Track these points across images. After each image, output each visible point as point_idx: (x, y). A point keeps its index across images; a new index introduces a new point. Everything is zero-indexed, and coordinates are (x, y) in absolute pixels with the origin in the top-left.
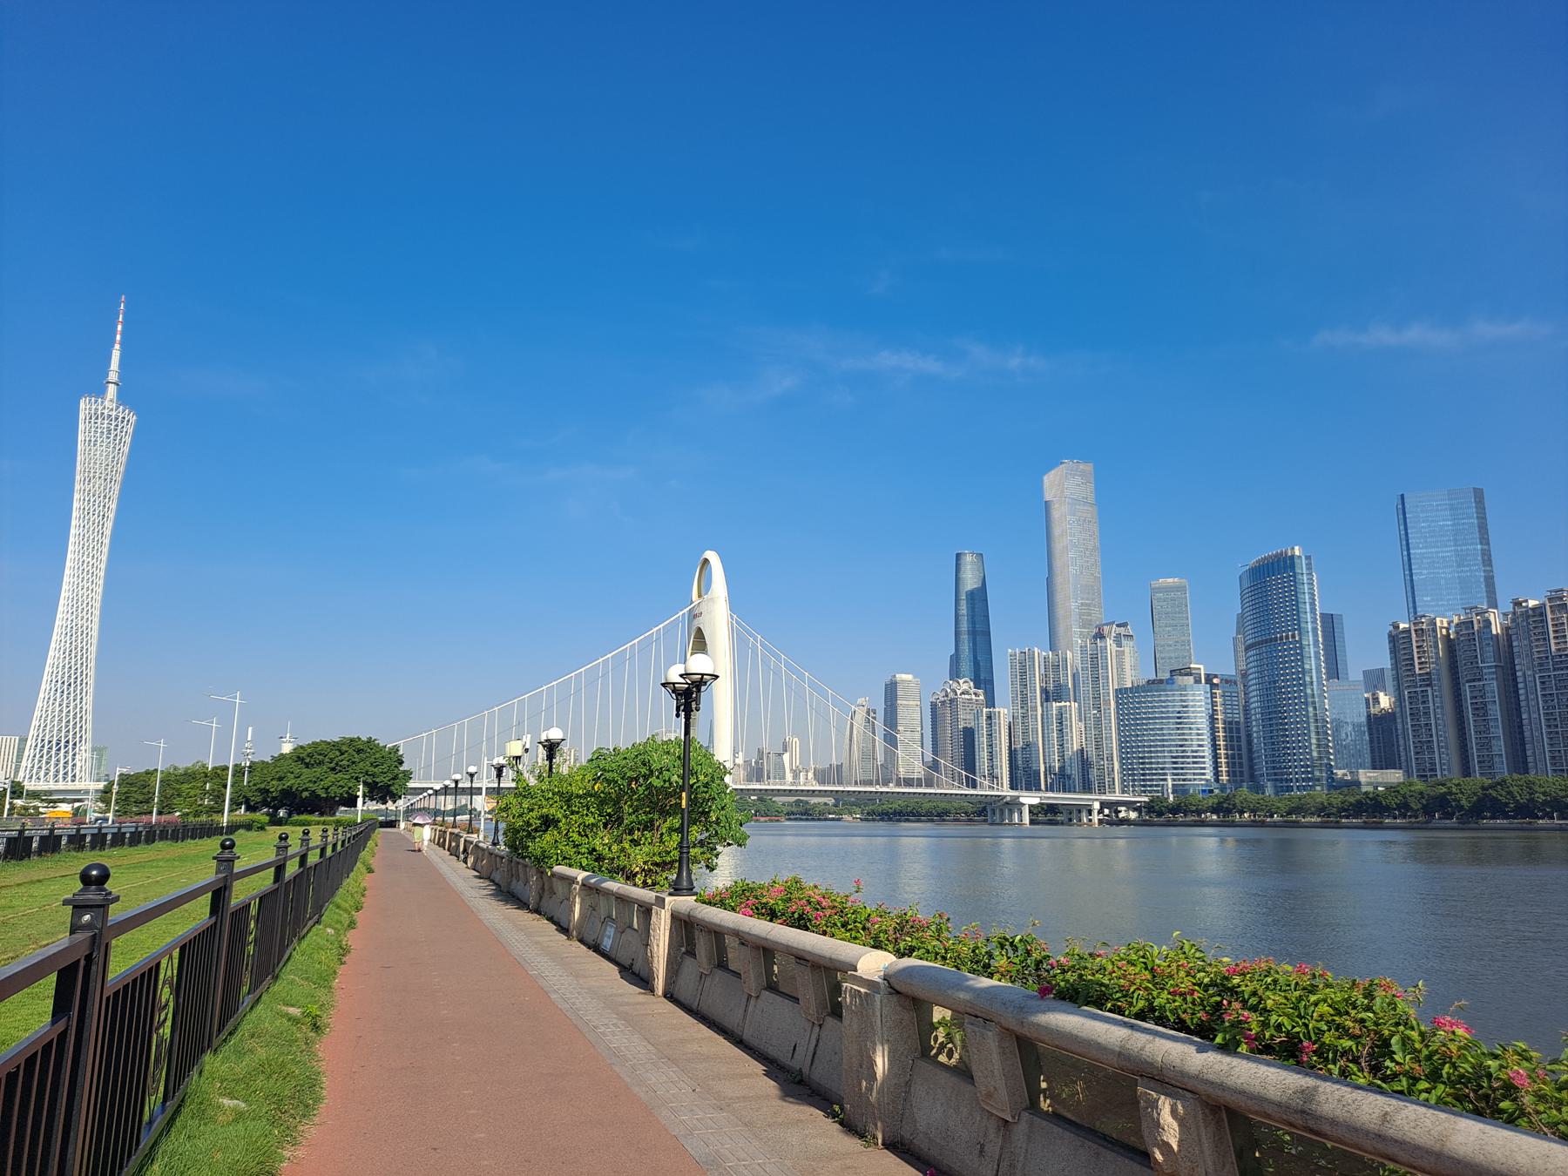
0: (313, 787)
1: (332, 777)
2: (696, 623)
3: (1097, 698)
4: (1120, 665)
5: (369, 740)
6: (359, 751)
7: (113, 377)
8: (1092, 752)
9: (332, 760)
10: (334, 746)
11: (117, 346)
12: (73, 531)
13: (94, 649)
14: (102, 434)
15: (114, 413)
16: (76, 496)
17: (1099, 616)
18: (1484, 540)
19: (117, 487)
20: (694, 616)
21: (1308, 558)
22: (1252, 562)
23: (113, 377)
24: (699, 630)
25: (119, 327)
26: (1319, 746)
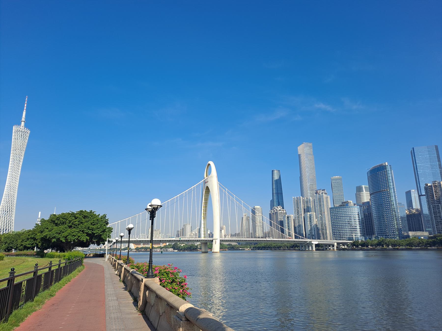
0: (58, 236)
1: (69, 230)
2: (206, 185)
3: (321, 211)
4: (327, 201)
5: (91, 212)
6: (85, 217)
7: (23, 119)
8: (319, 226)
9: (70, 221)
10: (73, 215)
11: (25, 111)
12: (10, 165)
13: (15, 201)
14: (19, 137)
15: (23, 130)
16: (11, 155)
17: (316, 187)
18: (439, 161)
19: (24, 152)
20: (205, 182)
21: (390, 166)
22: (371, 167)
23: (23, 119)
24: (207, 187)
25: (26, 105)
26: (397, 224)
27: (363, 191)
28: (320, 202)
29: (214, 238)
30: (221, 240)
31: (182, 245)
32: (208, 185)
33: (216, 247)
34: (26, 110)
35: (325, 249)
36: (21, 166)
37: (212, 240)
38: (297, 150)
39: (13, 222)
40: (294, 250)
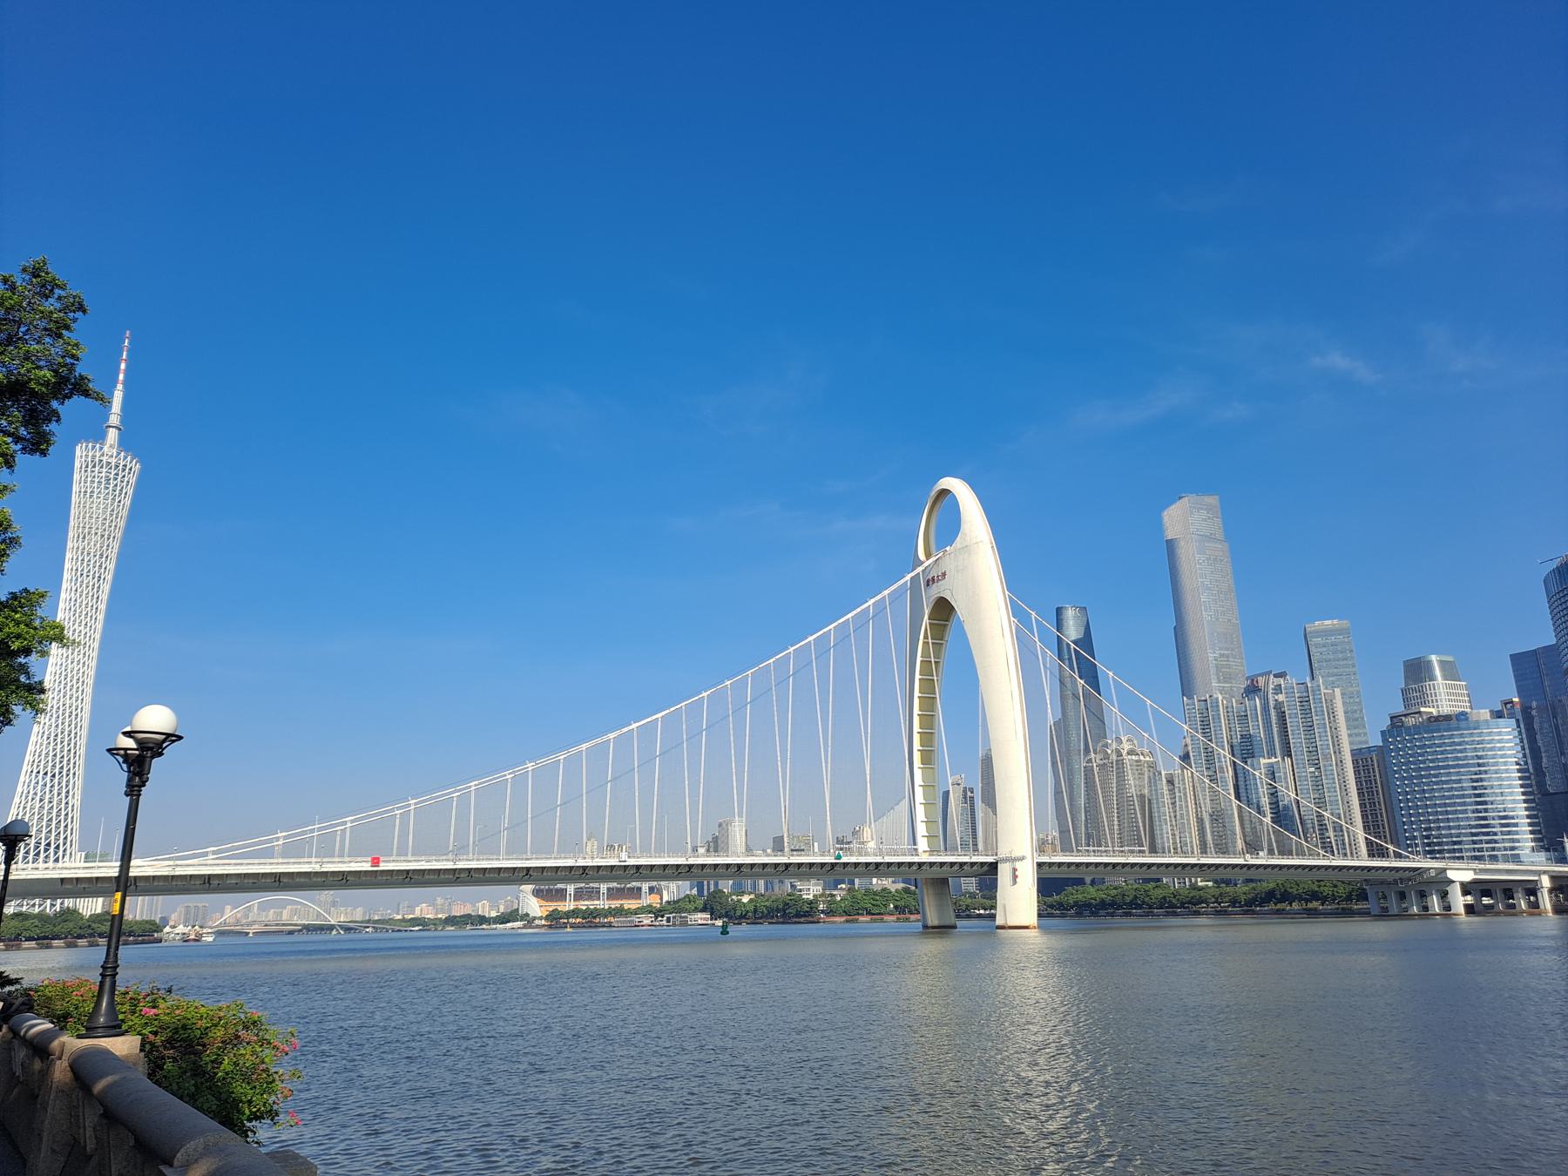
7: (114, 420)
11: (120, 387)
13: (84, 732)
15: (113, 461)
23: (114, 420)
25: (123, 366)
27: (1432, 678)
28: (1307, 712)
30: (1040, 865)
31: (745, 899)
32: (949, 590)
33: (1019, 901)
34: (125, 383)
36: (104, 597)
37: (993, 867)
38: (1159, 526)
39: (77, 815)
40: (1278, 912)
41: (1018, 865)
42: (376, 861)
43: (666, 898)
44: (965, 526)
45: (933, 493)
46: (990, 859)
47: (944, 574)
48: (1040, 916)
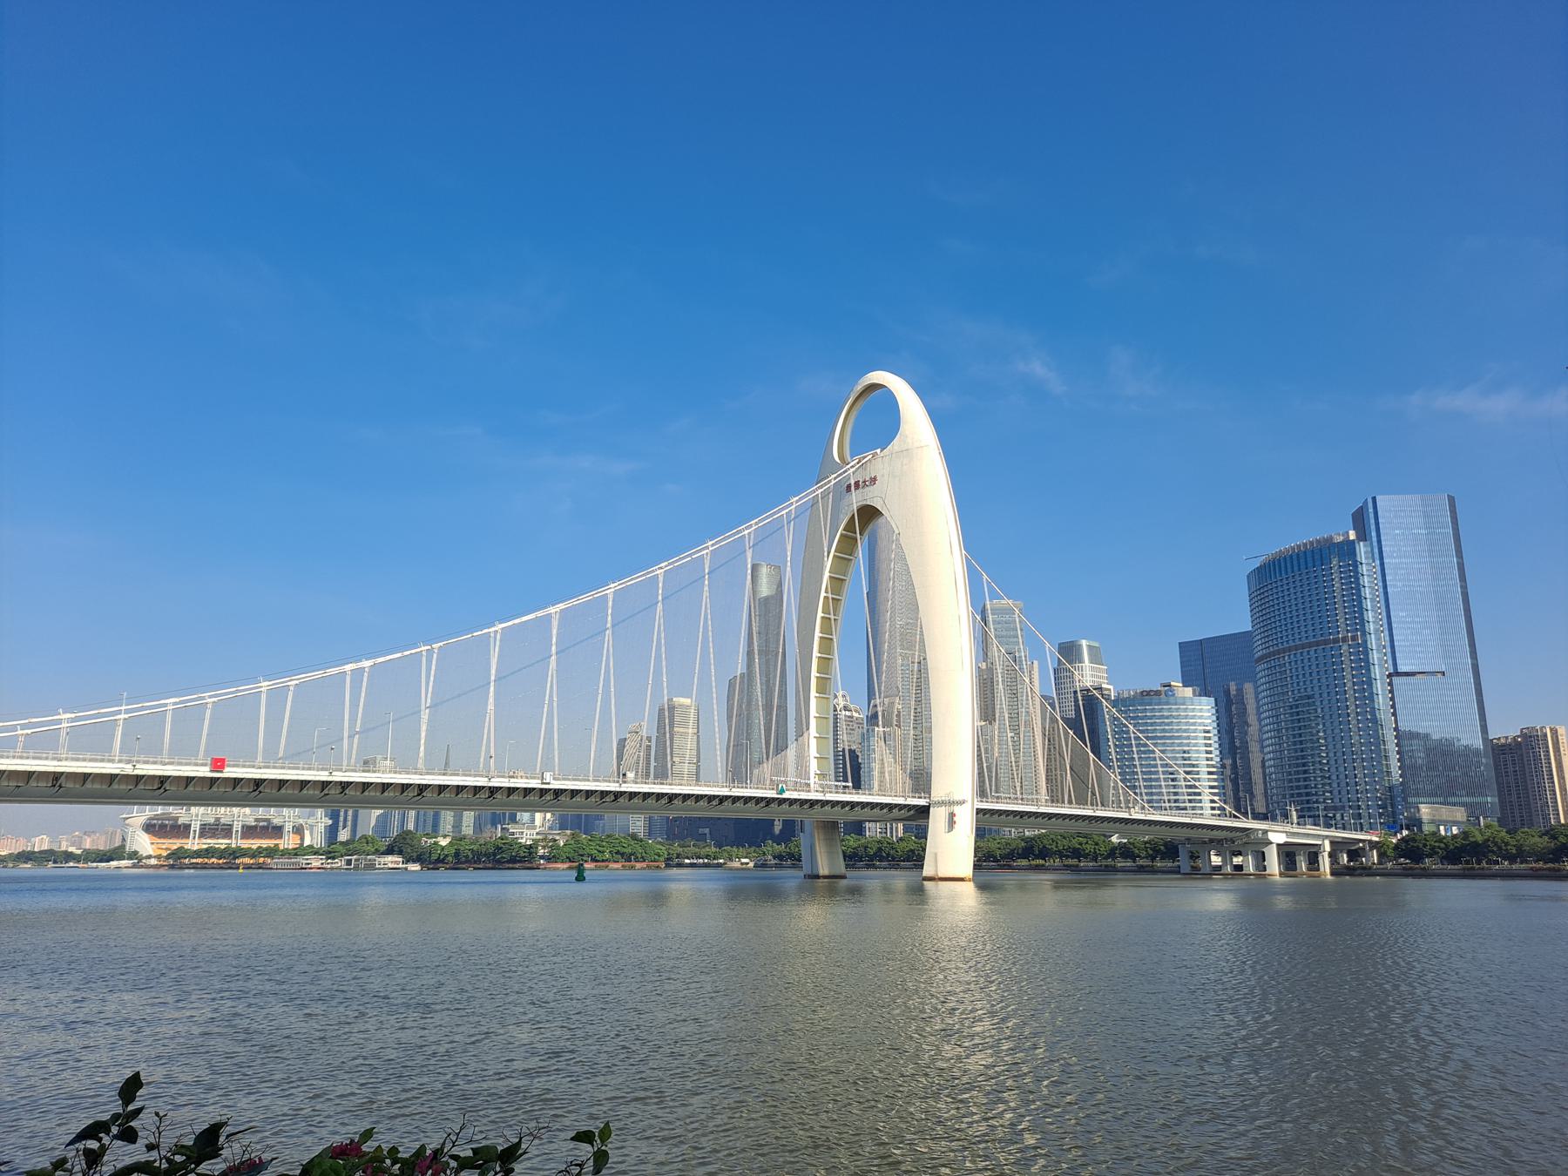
27: (1081, 661)
29: (938, 792)
30: (979, 811)
33: (952, 849)
35: (1186, 868)
37: (924, 811)
40: (1010, 867)
41: (957, 809)
42: (218, 764)
43: (307, 842)
44: (905, 427)
45: (859, 388)
46: (922, 802)
47: (874, 480)
48: (976, 867)
